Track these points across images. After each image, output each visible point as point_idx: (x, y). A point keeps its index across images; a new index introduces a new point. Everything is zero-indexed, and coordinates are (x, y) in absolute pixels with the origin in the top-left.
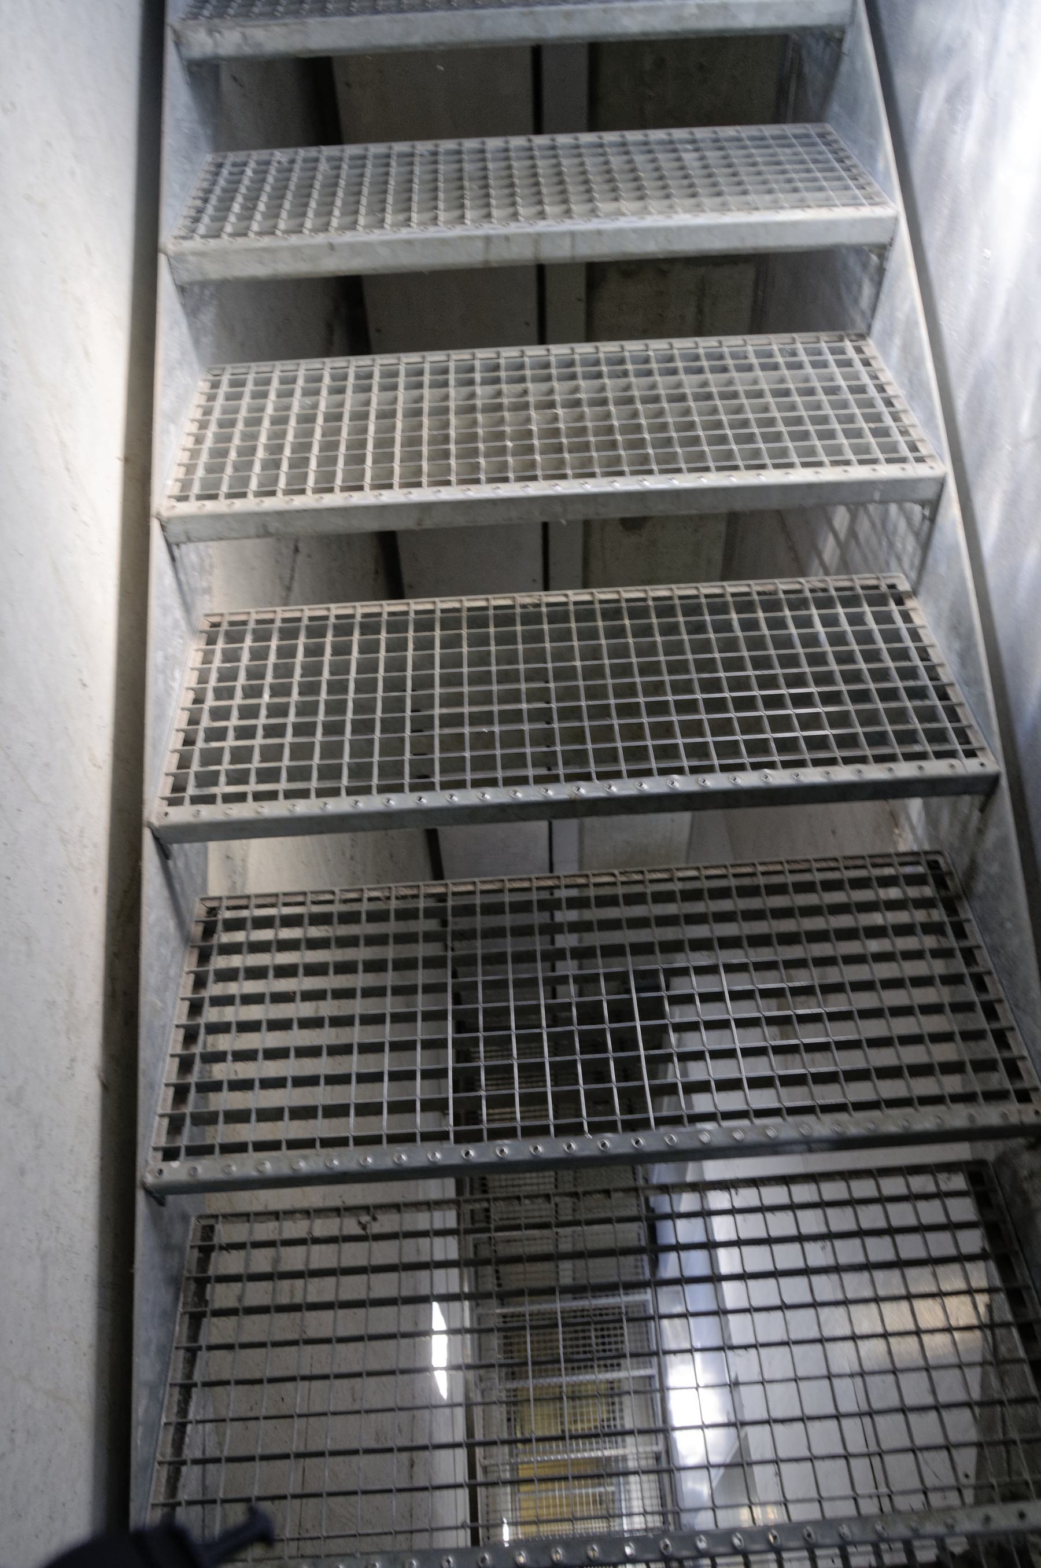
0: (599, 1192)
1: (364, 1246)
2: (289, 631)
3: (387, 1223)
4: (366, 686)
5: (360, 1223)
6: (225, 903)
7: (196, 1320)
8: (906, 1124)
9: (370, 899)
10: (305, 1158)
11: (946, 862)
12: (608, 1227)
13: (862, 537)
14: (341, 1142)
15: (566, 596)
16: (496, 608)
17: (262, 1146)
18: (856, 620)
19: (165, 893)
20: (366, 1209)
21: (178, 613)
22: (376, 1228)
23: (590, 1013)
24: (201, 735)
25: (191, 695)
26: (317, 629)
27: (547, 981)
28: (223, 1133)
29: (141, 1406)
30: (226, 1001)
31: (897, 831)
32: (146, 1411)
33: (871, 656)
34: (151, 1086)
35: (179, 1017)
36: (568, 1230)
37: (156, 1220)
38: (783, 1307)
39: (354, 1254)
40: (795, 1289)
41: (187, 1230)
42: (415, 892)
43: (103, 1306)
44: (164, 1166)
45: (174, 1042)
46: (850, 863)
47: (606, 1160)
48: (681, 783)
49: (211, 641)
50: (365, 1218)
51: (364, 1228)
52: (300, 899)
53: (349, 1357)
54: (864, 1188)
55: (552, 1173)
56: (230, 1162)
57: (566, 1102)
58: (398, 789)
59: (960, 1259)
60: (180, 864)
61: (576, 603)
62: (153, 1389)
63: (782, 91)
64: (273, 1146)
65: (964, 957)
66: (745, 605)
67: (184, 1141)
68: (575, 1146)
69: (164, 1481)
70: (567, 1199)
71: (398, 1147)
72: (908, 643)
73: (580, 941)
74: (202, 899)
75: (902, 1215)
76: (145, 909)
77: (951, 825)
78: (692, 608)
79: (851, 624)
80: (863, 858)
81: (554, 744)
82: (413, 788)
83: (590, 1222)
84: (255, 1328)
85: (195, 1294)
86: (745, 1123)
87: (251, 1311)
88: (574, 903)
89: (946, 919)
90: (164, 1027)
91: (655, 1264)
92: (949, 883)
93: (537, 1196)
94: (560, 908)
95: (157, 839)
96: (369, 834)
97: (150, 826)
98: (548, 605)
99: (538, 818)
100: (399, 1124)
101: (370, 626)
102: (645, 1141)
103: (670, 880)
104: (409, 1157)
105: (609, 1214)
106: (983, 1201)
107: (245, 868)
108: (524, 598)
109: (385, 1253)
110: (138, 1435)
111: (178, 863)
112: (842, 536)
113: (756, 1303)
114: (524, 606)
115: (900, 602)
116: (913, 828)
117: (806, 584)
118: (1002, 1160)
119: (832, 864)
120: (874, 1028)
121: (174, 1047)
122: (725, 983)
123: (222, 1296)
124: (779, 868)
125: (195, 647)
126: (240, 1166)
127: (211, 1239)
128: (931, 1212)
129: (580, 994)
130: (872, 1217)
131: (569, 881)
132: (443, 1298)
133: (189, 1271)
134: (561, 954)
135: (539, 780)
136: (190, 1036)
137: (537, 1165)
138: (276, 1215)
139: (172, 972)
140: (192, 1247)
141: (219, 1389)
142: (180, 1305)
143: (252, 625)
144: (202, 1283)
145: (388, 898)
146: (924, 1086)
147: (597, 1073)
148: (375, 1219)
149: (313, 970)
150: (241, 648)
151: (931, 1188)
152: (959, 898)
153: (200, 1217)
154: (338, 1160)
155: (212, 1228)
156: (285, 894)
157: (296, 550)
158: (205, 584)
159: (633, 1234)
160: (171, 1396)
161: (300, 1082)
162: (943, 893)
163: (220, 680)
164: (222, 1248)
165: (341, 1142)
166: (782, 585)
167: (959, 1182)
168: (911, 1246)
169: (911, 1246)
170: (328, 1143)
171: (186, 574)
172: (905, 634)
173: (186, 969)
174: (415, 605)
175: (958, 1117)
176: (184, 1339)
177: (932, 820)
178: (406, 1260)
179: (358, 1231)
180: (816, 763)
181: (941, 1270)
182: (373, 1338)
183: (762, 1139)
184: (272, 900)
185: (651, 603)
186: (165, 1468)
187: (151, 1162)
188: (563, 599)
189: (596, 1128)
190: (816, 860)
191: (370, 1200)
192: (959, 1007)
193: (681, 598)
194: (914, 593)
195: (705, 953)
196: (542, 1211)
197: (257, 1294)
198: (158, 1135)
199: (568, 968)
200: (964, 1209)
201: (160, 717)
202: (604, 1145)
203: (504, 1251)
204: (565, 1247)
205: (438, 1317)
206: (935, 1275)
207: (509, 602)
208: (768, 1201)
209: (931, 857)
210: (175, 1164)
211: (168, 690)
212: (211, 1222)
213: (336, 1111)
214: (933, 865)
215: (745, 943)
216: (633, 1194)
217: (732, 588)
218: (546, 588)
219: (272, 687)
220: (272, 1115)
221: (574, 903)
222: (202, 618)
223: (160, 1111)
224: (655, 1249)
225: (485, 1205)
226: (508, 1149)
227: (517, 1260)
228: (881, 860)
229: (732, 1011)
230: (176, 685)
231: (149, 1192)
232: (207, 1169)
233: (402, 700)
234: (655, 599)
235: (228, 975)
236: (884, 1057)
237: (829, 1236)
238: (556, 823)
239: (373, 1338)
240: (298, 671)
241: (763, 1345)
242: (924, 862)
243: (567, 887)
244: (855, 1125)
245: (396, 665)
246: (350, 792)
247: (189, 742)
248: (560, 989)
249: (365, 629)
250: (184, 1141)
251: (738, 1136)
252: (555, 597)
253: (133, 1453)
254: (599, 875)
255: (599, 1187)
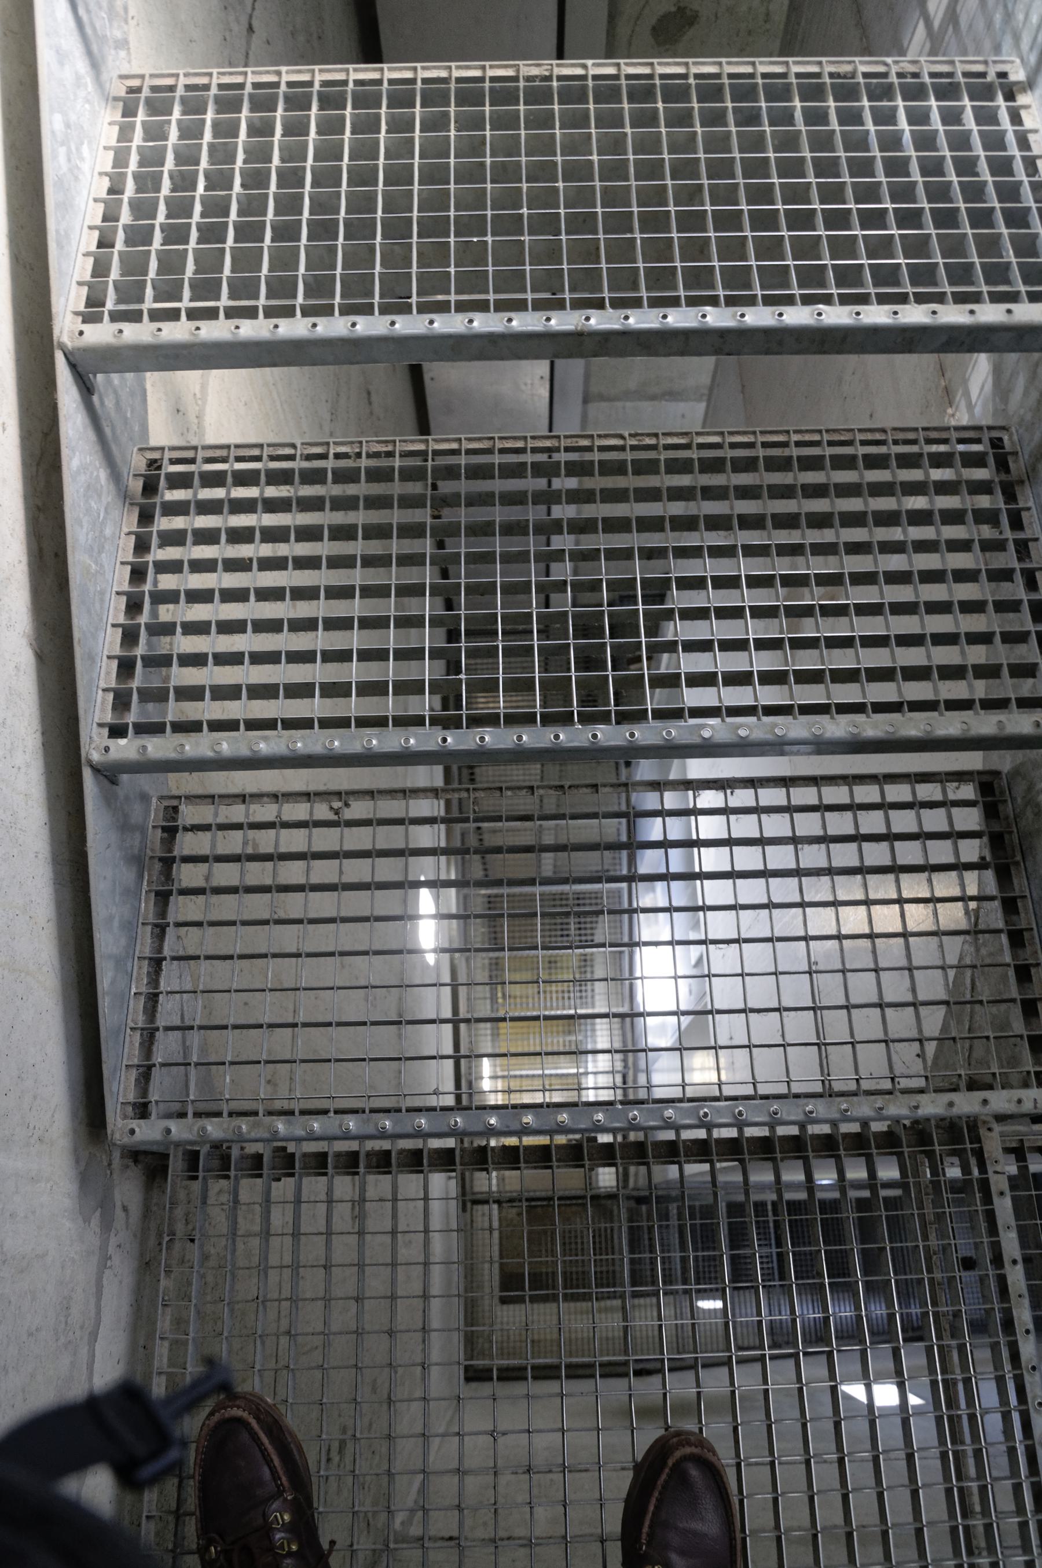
0: (587, 786)
1: (335, 832)
2: (229, 101)
3: (358, 809)
4: (327, 178)
5: (331, 808)
6: (167, 455)
7: (163, 898)
8: (928, 728)
9: (337, 456)
10: (265, 739)
11: (1011, 439)
12: (595, 822)
13: (964, 21)
14: (305, 724)
15: (585, 67)
16: (493, 79)
17: (218, 726)
18: (951, 117)
19: (91, 435)
20: (338, 794)
21: (81, 65)
22: (348, 814)
23: (587, 627)
24: (120, 236)
25: (106, 183)
26: (264, 100)
27: (541, 588)
28: (174, 710)
29: (106, 977)
30: (173, 567)
31: (950, 411)
32: (113, 982)
33: (966, 166)
34: (91, 658)
35: (120, 584)
36: (552, 823)
37: (108, 800)
38: (770, 906)
39: (326, 840)
40: (784, 889)
41: (147, 812)
42: (390, 448)
43: (58, 882)
44: (112, 743)
45: (116, 611)
46: (901, 436)
47: (595, 754)
48: (716, 318)
49: (129, 111)
50: (337, 804)
51: (337, 812)
52: (256, 452)
53: (321, 938)
54: (867, 793)
55: (539, 766)
56: (184, 742)
57: (556, 689)
58: (366, 310)
59: (959, 867)
60: (110, 403)
61: (596, 77)
62: (119, 962)
63: (702, 252)
64: (231, 726)
65: (1017, 551)
66: (812, 90)
67: (132, 717)
68: (565, 737)
69: (137, 1045)
70: (552, 792)
71: (368, 731)
72: (1014, 150)
73: (579, 512)
74: (140, 449)
75: (903, 821)
76: (65, 452)
77: (1026, 393)
78: (744, 90)
79: (945, 122)
80: (916, 429)
81: (560, 234)
82: (385, 310)
83: (574, 817)
84: (226, 907)
85: (161, 873)
86: (751, 720)
87: (218, 891)
88: (575, 469)
89: (1002, 506)
90: (102, 593)
91: (632, 861)
92: (1011, 464)
93: (520, 788)
94: (558, 475)
95: (73, 366)
96: (331, 367)
97: (62, 347)
98: (560, 78)
99: (538, 357)
100: (370, 707)
101: (332, 98)
102: (644, 733)
103: (687, 447)
104: (379, 741)
105: (596, 810)
106: (991, 811)
107: (200, 425)
108: (529, 69)
109: (358, 839)
110: (105, 1004)
111: (106, 402)
112: (936, 24)
113: (742, 901)
114: (529, 79)
115: (1010, 96)
116: (970, 407)
117: (893, 65)
118: (1016, 772)
119: (878, 436)
120: (906, 624)
121: (115, 616)
122: (744, 567)
123: (189, 875)
124: (816, 437)
125: (108, 119)
126: (197, 746)
127: (175, 820)
128: (935, 820)
129: (575, 573)
130: (872, 822)
131: (569, 443)
132: (430, 884)
133: (152, 850)
134: (558, 556)
135: (539, 306)
136: (134, 606)
137: (520, 755)
138: (242, 798)
139: (108, 532)
140: (154, 827)
141: (192, 962)
142: (145, 883)
143: (180, 91)
144: (168, 862)
145: (359, 455)
146: (955, 690)
147: (589, 661)
148: (347, 805)
149: (272, 535)
150: (169, 122)
151: (938, 797)
152: (1021, 482)
153: (161, 798)
154: (302, 742)
155: (175, 809)
156: (237, 446)
157: (251, 29)
158: (118, 34)
159: (614, 829)
160: (140, 968)
161: (259, 658)
162: (1004, 477)
163: (141, 164)
164: (186, 829)
165: (305, 724)
166: (863, 65)
167: (968, 791)
168: (909, 853)
169: (909, 853)
170: (291, 724)
171: (88, 11)
172: (1011, 138)
173: (125, 530)
174: (391, 72)
175: (985, 724)
176: (151, 915)
177: (1001, 388)
178: (379, 846)
179: (331, 816)
180: (883, 299)
181: (936, 877)
182: (345, 920)
183: (769, 737)
184: (223, 453)
185: (691, 81)
186: (138, 1034)
187: (95, 738)
188: (580, 71)
189: (587, 719)
190: (860, 430)
191: (344, 786)
192: (1004, 607)
193: (731, 76)
194: (1029, 85)
195: (722, 533)
196: (524, 803)
197: (226, 874)
198: (103, 710)
199: (564, 571)
200: (970, 819)
201: (66, 206)
202: (595, 736)
203: (491, 841)
204: (548, 840)
205: (426, 900)
206: (930, 881)
207: (510, 73)
208: (763, 802)
209: (995, 434)
210: (123, 742)
211: (74, 172)
212: (175, 803)
213: (301, 691)
214: (996, 443)
215: (769, 523)
216: (623, 789)
217: (798, 66)
218: (560, 55)
219: (238, 227)
220: (231, 693)
221: (575, 469)
222: (115, 79)
223: (103, 684)
224: (634, 845)
225: (464, 795)
226: (490, 737)
227: (498, 850)
228: (938, 434)
229: (749, 598)
230: (86, 167)
231: (96, 770)
232: (157, 747)
233: (372, 198)
234: (697, 76)
235: (175, 538)
236: (912, 657)
237: (729, 842)
238: (559, 363)
239: (345, 920)
240: (240, 156)
241: (747, 941)
242: (986, 439)
243: (567, 449)
244: (872, 727)
245: (365, 151)
246: (306, 312)
247: (105, 243)
248: (554, 597)
249: (325, 101)
250: (132, 717)
251: (743, 733)
252: (569, 68)
253: (102, 1021)
254: (606, 436)
255: (588, 782)
